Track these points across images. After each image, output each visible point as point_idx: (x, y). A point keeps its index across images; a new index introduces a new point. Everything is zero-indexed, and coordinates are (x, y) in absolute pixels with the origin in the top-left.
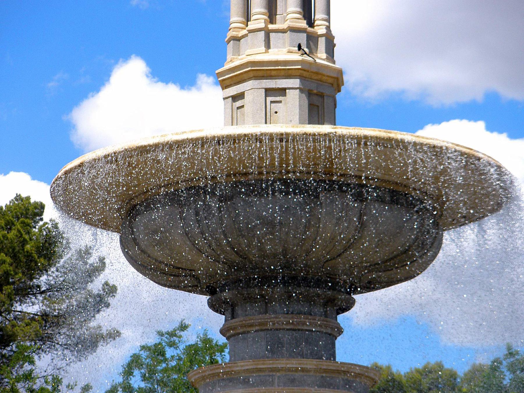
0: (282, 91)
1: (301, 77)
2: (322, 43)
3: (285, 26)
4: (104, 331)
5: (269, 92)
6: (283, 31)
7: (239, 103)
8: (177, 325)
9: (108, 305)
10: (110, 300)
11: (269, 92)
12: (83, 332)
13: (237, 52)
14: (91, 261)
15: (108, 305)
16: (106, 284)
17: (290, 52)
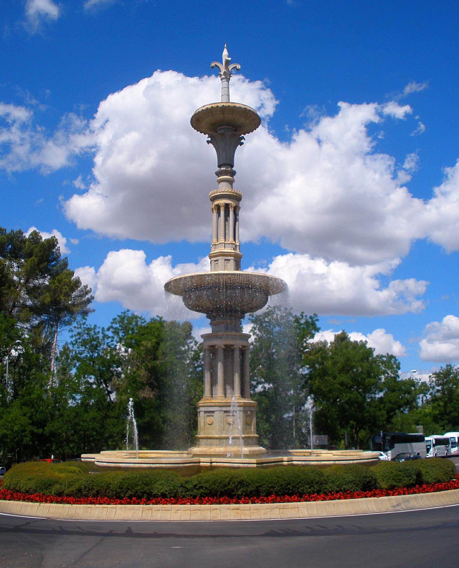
0: (229, 260)
1: (234, 256)
2: (238, 247)
3: (229, 242)
4: (91, 310)
5: (225, 260)
6: (229, 244)
7: (216, 262)
8: (126, 310)
9: (91, 302)
10: (92, 301)
11: (225, 260)
12: (85, 309)
13: (215, 248)
14: (87, 289)
15: (91, 302)
16: (91, 296)
17: (231, 250)
